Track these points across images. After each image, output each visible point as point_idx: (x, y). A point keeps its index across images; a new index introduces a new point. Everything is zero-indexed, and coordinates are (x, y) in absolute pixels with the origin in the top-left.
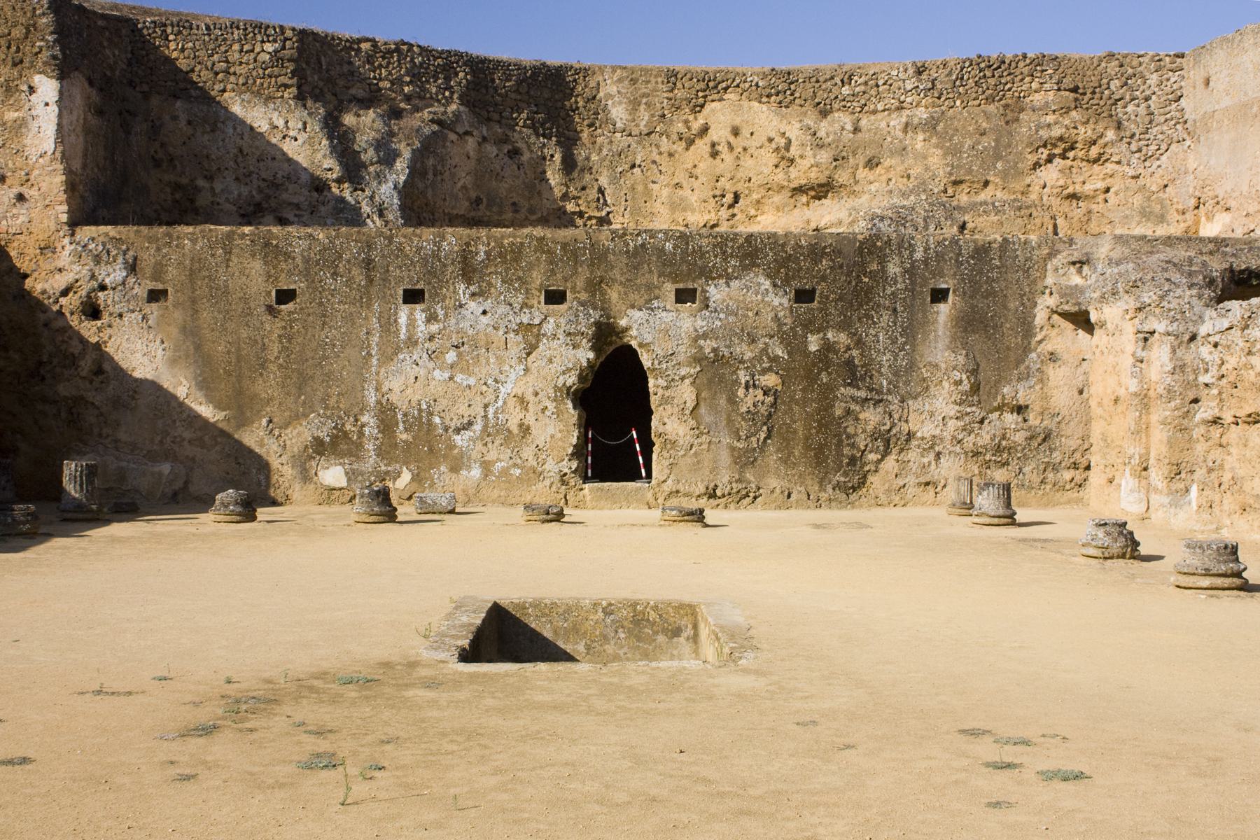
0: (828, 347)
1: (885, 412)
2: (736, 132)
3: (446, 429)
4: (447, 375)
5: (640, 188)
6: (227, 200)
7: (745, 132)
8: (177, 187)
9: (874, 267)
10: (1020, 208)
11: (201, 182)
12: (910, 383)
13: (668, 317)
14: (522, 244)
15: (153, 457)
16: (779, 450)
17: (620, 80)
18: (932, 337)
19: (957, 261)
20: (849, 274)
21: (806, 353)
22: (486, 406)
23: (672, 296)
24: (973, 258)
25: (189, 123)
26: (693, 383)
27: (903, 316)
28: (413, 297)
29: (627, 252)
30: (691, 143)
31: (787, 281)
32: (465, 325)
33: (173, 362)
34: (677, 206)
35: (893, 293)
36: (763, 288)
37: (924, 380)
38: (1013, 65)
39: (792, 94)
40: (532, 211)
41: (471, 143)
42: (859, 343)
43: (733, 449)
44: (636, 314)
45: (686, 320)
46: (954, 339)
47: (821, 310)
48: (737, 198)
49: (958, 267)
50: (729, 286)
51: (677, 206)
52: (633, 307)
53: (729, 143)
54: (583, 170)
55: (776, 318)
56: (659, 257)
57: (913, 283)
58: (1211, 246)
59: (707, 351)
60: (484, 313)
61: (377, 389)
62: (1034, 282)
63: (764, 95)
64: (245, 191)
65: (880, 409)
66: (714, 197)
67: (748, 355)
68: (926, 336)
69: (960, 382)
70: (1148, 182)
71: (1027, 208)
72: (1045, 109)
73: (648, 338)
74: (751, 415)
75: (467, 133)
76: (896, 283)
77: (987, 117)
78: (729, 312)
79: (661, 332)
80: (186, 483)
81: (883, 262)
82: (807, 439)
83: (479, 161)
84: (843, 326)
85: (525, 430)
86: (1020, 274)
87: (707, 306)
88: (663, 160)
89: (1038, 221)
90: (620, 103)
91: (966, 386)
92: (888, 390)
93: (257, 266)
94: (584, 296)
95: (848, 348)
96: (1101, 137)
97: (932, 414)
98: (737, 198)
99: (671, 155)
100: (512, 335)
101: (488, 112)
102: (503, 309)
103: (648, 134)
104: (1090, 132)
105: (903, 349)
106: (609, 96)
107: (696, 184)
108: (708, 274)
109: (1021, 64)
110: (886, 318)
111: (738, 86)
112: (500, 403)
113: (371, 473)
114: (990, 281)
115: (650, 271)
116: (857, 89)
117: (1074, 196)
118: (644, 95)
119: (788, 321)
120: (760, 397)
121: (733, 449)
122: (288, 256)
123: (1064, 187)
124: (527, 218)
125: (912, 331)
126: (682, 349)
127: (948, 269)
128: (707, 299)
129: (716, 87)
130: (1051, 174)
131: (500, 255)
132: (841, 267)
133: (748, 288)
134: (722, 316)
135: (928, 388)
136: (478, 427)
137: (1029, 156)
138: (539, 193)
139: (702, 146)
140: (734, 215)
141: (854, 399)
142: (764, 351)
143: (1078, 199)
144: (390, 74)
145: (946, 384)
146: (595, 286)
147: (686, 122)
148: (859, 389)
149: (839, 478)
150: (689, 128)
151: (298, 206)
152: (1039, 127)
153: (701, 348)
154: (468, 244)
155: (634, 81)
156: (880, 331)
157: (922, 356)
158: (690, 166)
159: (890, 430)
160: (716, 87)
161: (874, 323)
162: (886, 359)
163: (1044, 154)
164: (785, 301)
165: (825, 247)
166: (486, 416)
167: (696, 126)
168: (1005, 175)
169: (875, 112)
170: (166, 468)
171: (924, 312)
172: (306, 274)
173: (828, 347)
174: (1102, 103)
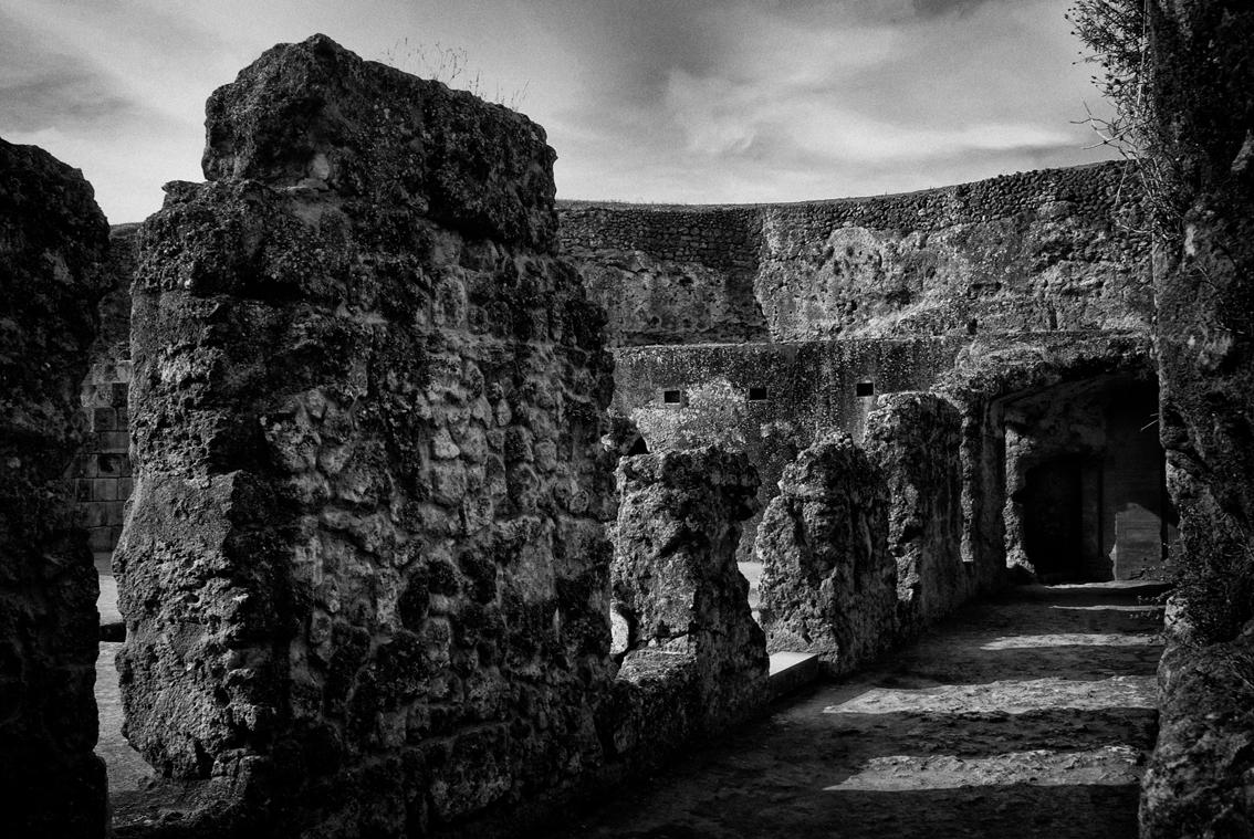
0: (775, 434)
2: (850, 252)
5: (786, 302)
7: (856, 253)
9: (811, 368)
10: (1022, 306)
13: (659, 413)
17: (776, 218)
18: (858, 424)
19: (878, 360)
20: (791, 376)
21: (759, 439)
23: (662, 397)
24: (891, 357)
27: (835, 408)
30: (822, 263)
31: (744, 383)
34: (813, 314)
35: (826, 389)
36: (726, 389)
38: (1027, 181)
39: (885, 219)
40: (701, 325)
41: (647, 279)
42: (800, 430)
44: (639, 412)
45: (672, 416)
47: (770, 404)
48: (854, 306)
50: (701, 388)
51: (813, 314)
52: (636, 406)
53: (846, 262)
56: (653, 368)
57: (842, 380)
63: (864, 221)
66: (838, 306)
70: (1137, 275)
71: (1028, 305)
72: (1047, 219)
73: (647, 429)
75: (643, 270)
76: (828, 380)
78: (704, 409)
81: (818, 364)
83: (655, 290)
84: (789, 416)
86: (931, 369)
87: (687, 405)
88: (803, 279)
89: (1038, 315)
90: (775, 235)
95: (791, 434)
98: (854, 306)
99: (808, 274)
103: (793, 259)
104: (1082, 235)
106: (768, 230)
107: (826, 296)
108: (685, 379)
109: (1033, 180)
111: (851, 215)
114: (906, 376)
116: (929, 211)
117: (1071, 293)
119: (745, 414)
124: (697, 331)
127: (871, 368)
128: (687, 399)
129: (838, 216)
130: (1053, 275)
132: (785, 370)
133: (715, 389)
134: (697, 411)
138: (708, 311)
139: (829, 265)
140: (853, 320)
143: (1078, 294)
144: (579, 233)
147: (818, 247)
150: (821, 252)
152: (1041, 234)
153: (684, 436)
155: (785, 217)
160: (838, 216)
161: (812, 414)
163: (1046, 256)
164: (742, 399)
165: (773, 355)
167: (825, 249)
168: (1011, 277)
169: (939, 229)
173: (775, 434)
174: (1095, 208)
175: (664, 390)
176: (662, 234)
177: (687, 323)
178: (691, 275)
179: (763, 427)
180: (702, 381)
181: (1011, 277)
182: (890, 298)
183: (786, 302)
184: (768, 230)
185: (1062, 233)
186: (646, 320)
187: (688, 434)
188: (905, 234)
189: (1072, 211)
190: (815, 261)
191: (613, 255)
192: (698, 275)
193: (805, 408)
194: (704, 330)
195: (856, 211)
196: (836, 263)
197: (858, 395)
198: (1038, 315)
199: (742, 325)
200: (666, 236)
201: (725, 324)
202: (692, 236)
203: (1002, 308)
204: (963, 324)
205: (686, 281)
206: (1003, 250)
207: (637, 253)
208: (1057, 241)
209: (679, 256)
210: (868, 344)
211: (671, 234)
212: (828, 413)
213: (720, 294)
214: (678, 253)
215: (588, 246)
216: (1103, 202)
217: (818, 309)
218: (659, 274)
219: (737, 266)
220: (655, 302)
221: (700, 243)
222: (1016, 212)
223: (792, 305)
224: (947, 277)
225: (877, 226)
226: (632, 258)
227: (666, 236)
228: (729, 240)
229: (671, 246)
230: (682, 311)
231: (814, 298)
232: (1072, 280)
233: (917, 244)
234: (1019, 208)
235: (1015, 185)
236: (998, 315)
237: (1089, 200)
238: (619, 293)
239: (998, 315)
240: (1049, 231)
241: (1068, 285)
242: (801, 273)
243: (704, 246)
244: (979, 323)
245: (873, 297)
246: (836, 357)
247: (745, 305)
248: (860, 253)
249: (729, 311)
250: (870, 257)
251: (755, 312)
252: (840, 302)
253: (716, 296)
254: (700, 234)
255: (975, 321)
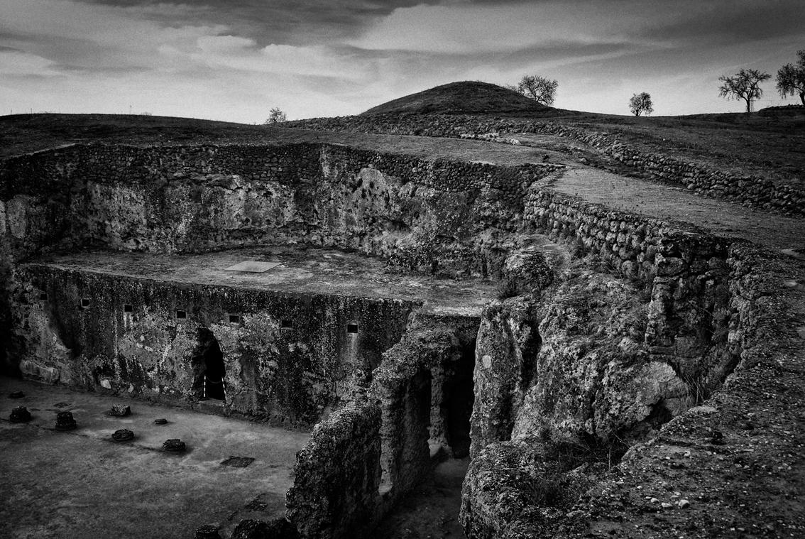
0: (298, 350)
1: (325, 386)
2: (372, 185)
3: (145, 369)
4: (142, 346)
6: (117, 231)
7: (376, 186)
8: (99, 224)
9: (319, 312)
11: (107, 222)
12: (338, 372)
14: (167, 289)
15: (48, 365)
16: (278, 398)
17: (328, 152)
20: (307, 315)
21: (288, 353)
22: (158, 361)
25: (102, 194)
26: (239, 361)
27: (334, 338)
28: (128, 309)
29: (209, 296)
30: (355, 189)
31: (278, 316)
32: (146, 324)
33: (51, 326)
34: (350, 221)
37: (345, 371)
40: (278, 223)
41: (241, 193)
42: (312, 350)
43: (258, 395)
46: (359, 351)
47: (294, 332)
48: (374, 221)
49: (361, 315)
51: (350, 221)
52: (213, 322)
53: (369, 191)
54: (306, 200)
55: (273, 334)
58: (471, 323)
59: (244, 347)
60: (153, 320)
61: (118, 348)
62: (401, 325)
63: (381, 167)
64: (123, 227)
65: (322, 384)
66: (364, 219)
67: (262, 351)
68: (345, 348)
69: (360, 375)
74: (265, 379)
75: (238, 188)
76: (330, 321)
77: (459, 199)
79: (227, 333)
80: (59, 377)
81: (324, 310)
82: (290, 393)
83: (247, 201)
84: (305, 340)
85: (174, 374)
90: (327, 164)
91: (364, 377)
92: (326, 375)
93: (75, 288)
94: (193, 315)
96: (511, 217)
97: (347, 389)
98: (374, 221)
99: (347, 194)
100: (165, 331)
101: (252, 175)
102: (160, 319)
104: (505, 214)
105: (334, 355)
106: (323, 160)
108: (242, 310)
110: (325, 339)
112: (163, 361)
113: (119, 384)
114: (377, 323)
115: (218, 306)
117: (496, 250)
118: (337, 161)
120: (268, 371)
121: (258, 395)
122: (86, 285)
123: (492, 245)
124: (275, 227)
125: (339, 345)
126: (234, 344)
130: (486, 237)
131: (159, 293)
132: (303, 311)
134: (250, 331)
135: (345, 376)
136: (156, 370)
137: (475, 225)
139: (359, 190)
140: (373, 229)
141: (310, 378)
142: (269, 349)
145: (354, 376)
146: (196, 311)
147: (353, 177)
148: (312, 373)
149: (305, 415)
151: (143, 235)
152: (480, 209)
153: (242, 345)
154: (146, 287)
155: (333, 153)
156: (323, 345)
157: (343, 359)
158: (354, 201)
159: (327, 395)
162: (325, 359)
163: (482, 224)
165: (296, 300)
166: (158, 366)
168: (461, 235)
170: (51, 370)
171: (345, 336)
172: (92, 294)
173: (298, 350)
175: (230, 314)
176: (252, 162)
177: (269, 222)
178: (272, 190)
179: (290, 345)
180: (252, 313)
181: (461, 235)
182: (394, 223)
183: (333, 211)
184: (323, 160)
185: (493, 211)
186: (241, 220)
187: (245, 344)
188: (404, 182)
189: (500, 197)
190: (351, 186)
191: (218, 179)
192: (276, 190)
193: (315, 336)
194: (280, 226)
195: (376, 158)
196: (364, 191)
197: (349, 332)
198: (475, 263)
199: (305, 223)
200: (255, 164)
201: (294, 223)
202: (272, 163)
203: (454, 256)
204: (429, 264)
205: (268, 194)
206: (457, 215)
207: (234, 176)
208: (489, 216)
209: (264, 177)
210: (355, 300)
211: (258, 163)
212: (330, 342)
213: (290, 203)
214: (262, 175)
215: (201, 173)
216: (519, 193)
217: (352, 218)
218: (250, 190)
219: (303, 183)
220: (247, 209)
221: (278, 168)
222: (468, 189)
223: (336, 214)
224: (424, 224)
225: (388, 173)
226: (231, 181)
227: (255, 164)
228: (298, 165)
229: (258, 170)
230: (265, 214)
231: (350, 211)
232: (498, 242)
233: (410, 193)
234: (469, 187)
235: (467, 171)
236: (451, 260)
237: (511, 190)
238: (222, 205)
239: (451, 260)
240: (485, 209)
241: (495, 245)
242: (342, 193)
243: (280, 169)
244: (440, 263)
245: (386, 219)
246: (335, 306)
247: (307, 210)
248: (378, 188)
249: (296, 214)
250: (383, 193)
251: (313, 216)
252: (365, 216)
253: (288, 204)
254: (278, 162)
255: (437, 262)
